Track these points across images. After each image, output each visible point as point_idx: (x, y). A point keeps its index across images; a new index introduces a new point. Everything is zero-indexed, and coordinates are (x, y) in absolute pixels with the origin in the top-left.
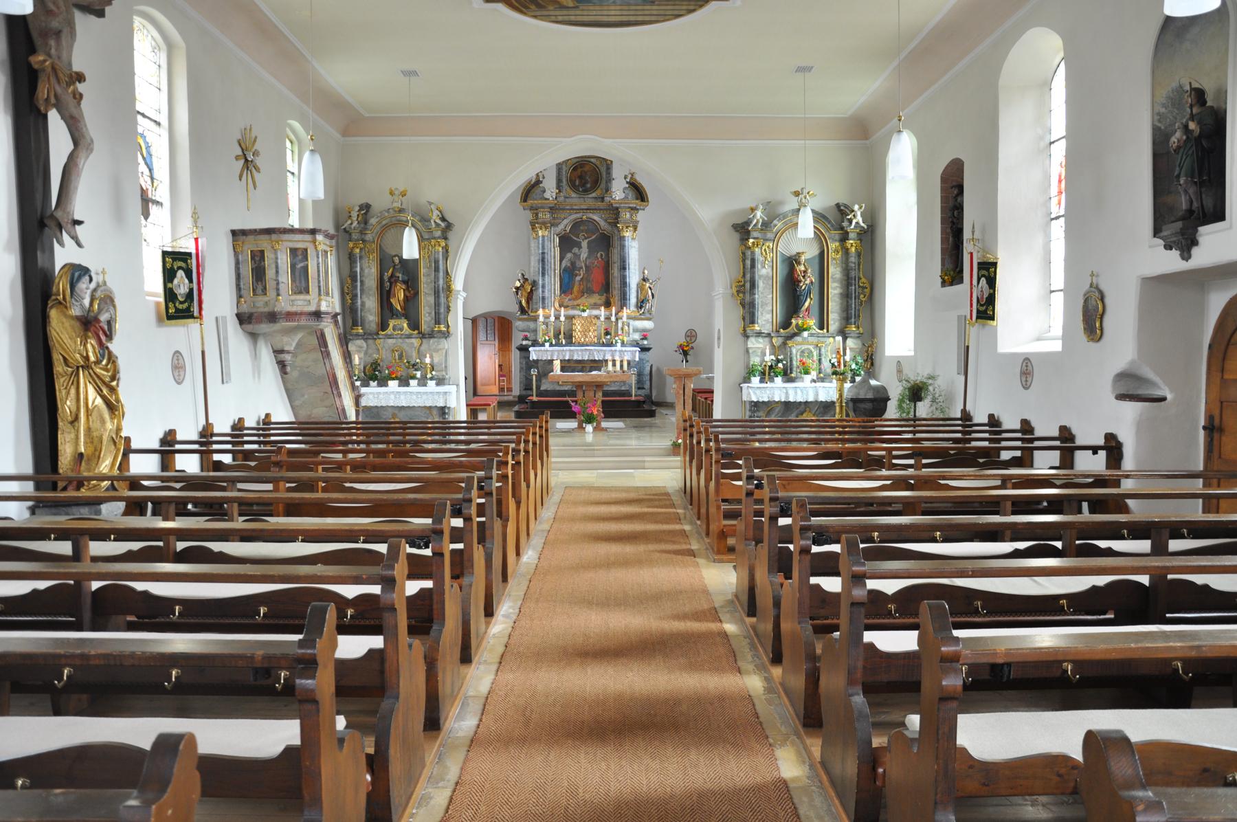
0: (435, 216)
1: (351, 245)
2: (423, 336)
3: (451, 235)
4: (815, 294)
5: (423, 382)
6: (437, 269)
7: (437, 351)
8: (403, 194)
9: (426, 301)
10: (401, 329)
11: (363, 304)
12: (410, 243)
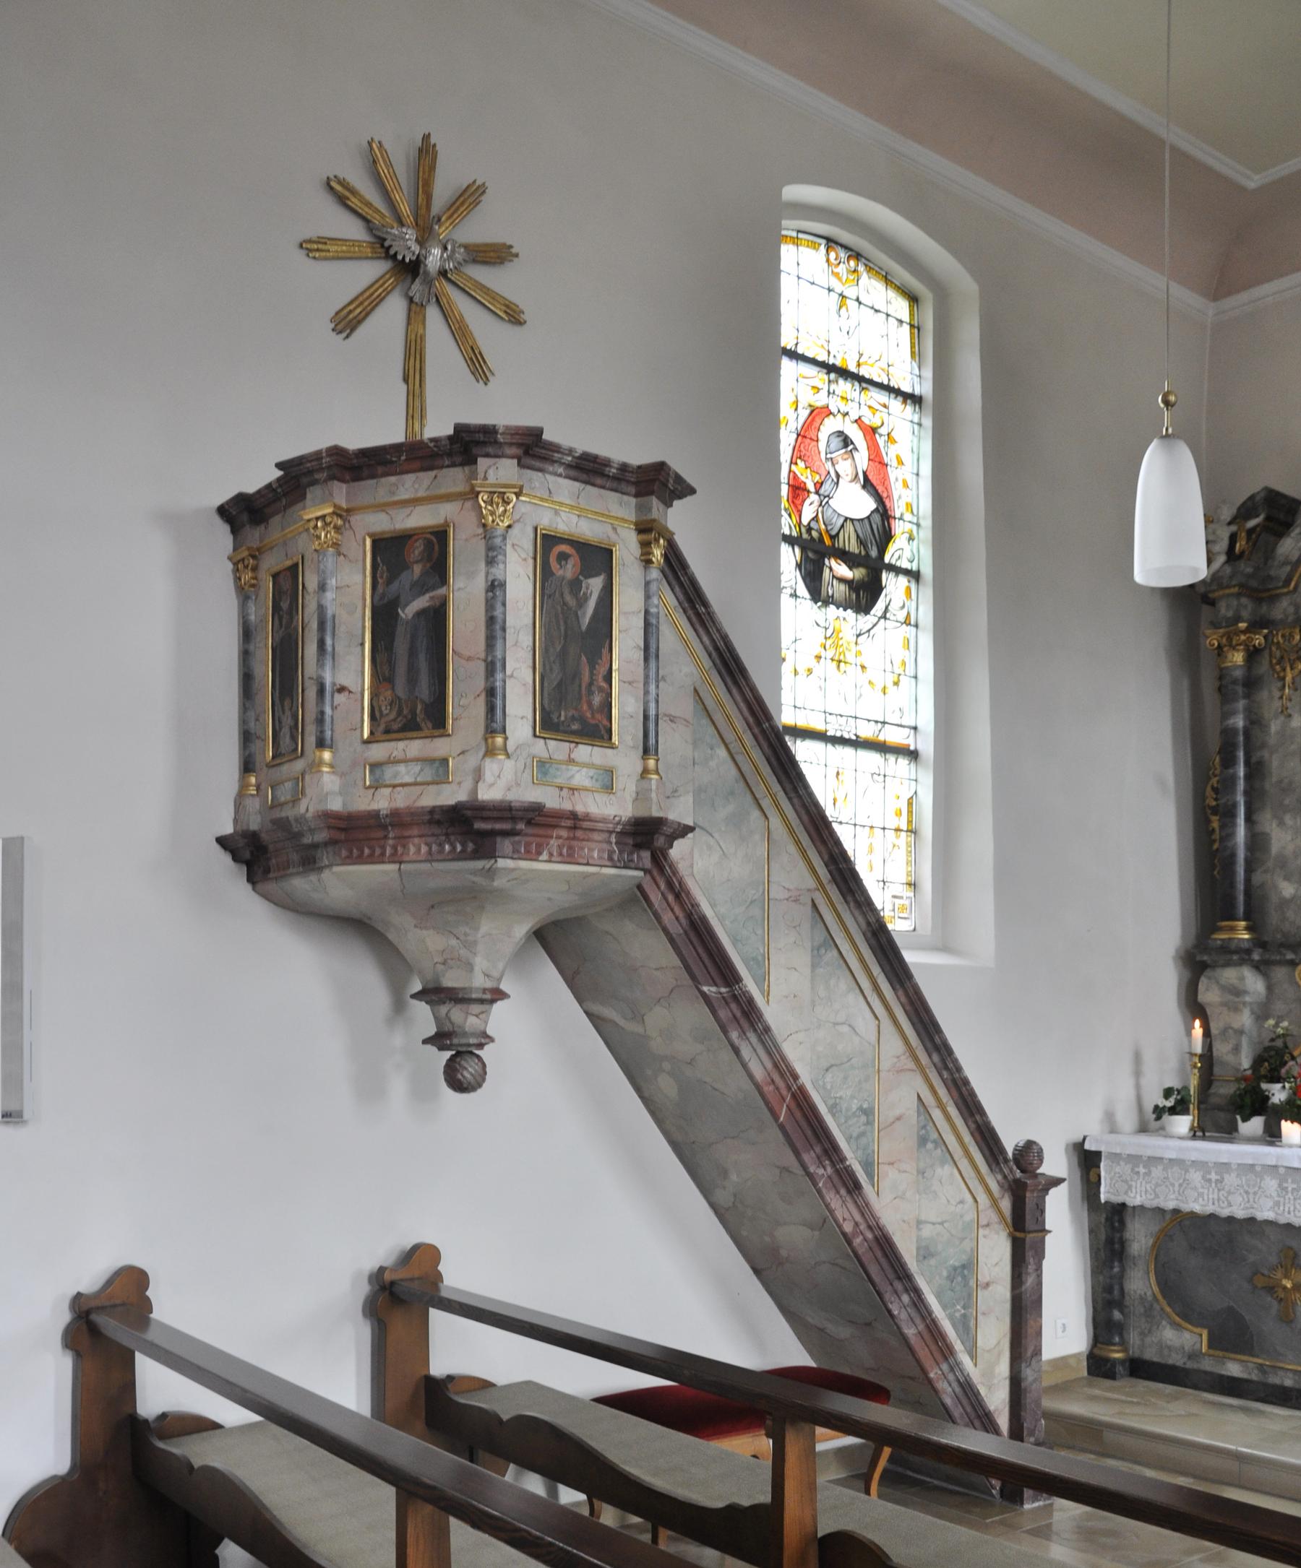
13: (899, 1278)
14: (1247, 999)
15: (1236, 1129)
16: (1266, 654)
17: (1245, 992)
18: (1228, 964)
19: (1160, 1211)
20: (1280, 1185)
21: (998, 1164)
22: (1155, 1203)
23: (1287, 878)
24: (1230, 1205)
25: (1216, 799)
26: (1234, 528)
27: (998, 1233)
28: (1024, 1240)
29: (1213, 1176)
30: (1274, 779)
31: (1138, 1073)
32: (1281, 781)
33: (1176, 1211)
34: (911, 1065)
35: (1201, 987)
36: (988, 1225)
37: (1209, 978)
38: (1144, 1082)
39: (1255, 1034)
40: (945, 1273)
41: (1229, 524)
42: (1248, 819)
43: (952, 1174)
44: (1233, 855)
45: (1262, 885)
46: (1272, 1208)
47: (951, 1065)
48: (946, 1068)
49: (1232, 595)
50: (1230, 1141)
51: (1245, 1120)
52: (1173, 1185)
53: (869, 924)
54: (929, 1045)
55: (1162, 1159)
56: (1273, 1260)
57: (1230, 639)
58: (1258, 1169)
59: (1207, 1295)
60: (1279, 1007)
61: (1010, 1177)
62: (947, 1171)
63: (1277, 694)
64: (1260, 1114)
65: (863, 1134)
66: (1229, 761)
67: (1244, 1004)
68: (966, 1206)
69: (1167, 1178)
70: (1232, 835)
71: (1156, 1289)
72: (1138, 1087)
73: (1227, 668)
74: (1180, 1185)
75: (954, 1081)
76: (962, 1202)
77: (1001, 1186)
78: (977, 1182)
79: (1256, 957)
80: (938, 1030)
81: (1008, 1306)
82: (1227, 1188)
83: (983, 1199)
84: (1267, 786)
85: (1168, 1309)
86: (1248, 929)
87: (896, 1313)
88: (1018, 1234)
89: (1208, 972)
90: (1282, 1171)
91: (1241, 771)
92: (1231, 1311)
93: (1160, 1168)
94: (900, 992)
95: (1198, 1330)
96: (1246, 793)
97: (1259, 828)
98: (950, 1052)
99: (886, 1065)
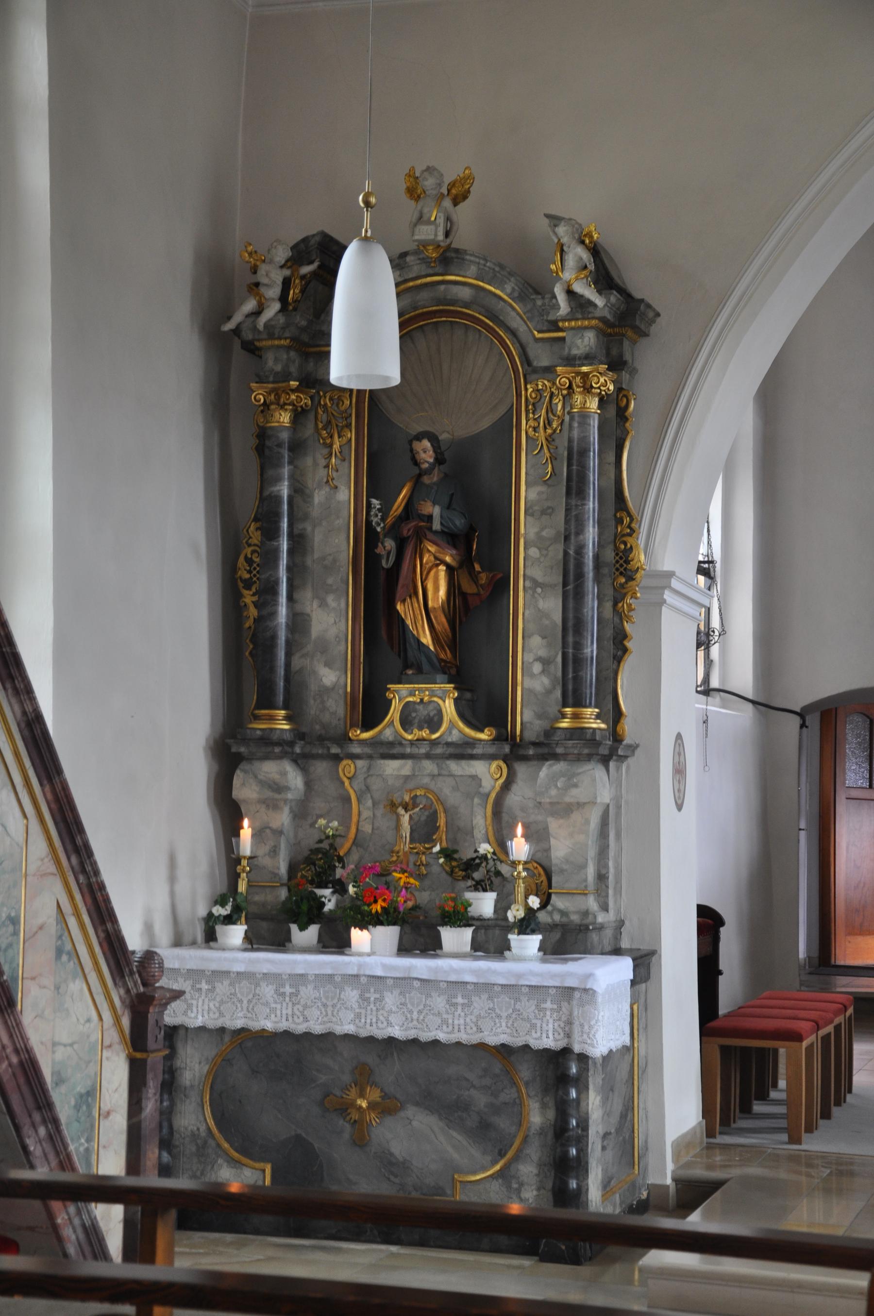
0: (571, 274)
1: (259, 396)
2: (515, 751)
3: (650, 359)
4: (120, 1012)
5: (491, 940)
6: (576, 488)
7: (565, 810)
8: (459, 194)
9: (533, 610)
10: (434, 722)
11: (299, 623)
12: (364, 316)
13: (39, 1108)
14: (290, 796)
15: (289, 939)
16: (312, 416)
17: (287, 788)
18: (266, 757)
19: (222, 1030)
20: (361, 996)
21: (123, 976)
22: (219, 1023)
23: (328, 664)
24: (306, 1020)
25: (250, 572)
26: (287, 272)
27: (118, 1055)
28: (144, 1062)
29: (288, 990)
30: (316, 556)
31: (172, 879)
32: (324, 558)
33: (243, 1030)
34: (52, 869)
35: (236, 782)
36: (110, 1046)
37: (245, 772)
38: (178, 888)
39: (291, 835)
40: (73, 1103)
41: (282, 267)
42: (290, 598)
43: (81, 990)
44: (274, 638)
45: (300, 671)
46: (352, 1021)
47: (89, 868)
48: (84, 871)
49: (279, 347)
50: (285, 951)
51: (302, 928)
52: (241, 1001)
53: (24, 713)
54: (70, 847)
55: (228, 972)
56: (347, 1078)
57: (278, 396)
58: (338, 979)
59: (273, 1124)
60: (318, 805)
61: (134, 991)
62: (77, 986)
63: (323, 462)
64: (314, 923)
65: (10, 946)
66: (270, 532)
67: (285, 801)
68: (92, 1025)
69: (235, 994)
70: (274, 614)
71: (211, 1122)
72: (172, 894)
73: (272, 428)
74: (249, 1001)
75: (90, 886)
76: (89, 1020)
77: (123, 1001)
78: (103, 997)
79: (298, 750)
80: (81, 830)
81: (123, 1138)
82: (302, 1002)
83: (107, 1015)
84: (309, 562)
85: (226, 1145)
86: (288, 718)
87: (32, 1149)
88: (138, 1055)
89: (244, 765)
90: (363, 980)
91: (284, 545)
92: (298, 1139)
93: (226, 983)
94: (47, 788)
95: (261, 1165)
96: (289, 569)
97: (298, 608)
98: (90, 854)
99: (32, 869)
